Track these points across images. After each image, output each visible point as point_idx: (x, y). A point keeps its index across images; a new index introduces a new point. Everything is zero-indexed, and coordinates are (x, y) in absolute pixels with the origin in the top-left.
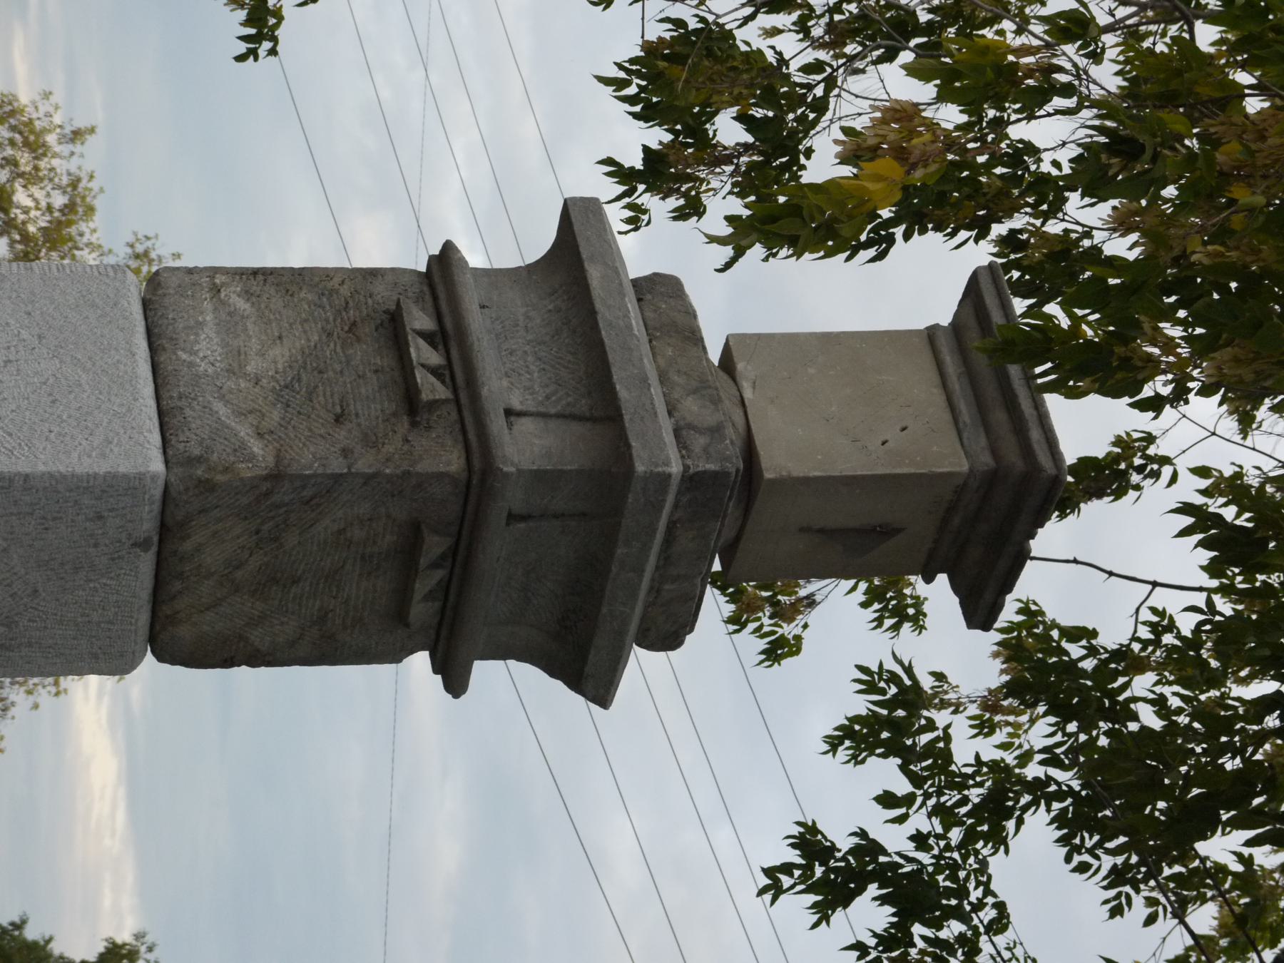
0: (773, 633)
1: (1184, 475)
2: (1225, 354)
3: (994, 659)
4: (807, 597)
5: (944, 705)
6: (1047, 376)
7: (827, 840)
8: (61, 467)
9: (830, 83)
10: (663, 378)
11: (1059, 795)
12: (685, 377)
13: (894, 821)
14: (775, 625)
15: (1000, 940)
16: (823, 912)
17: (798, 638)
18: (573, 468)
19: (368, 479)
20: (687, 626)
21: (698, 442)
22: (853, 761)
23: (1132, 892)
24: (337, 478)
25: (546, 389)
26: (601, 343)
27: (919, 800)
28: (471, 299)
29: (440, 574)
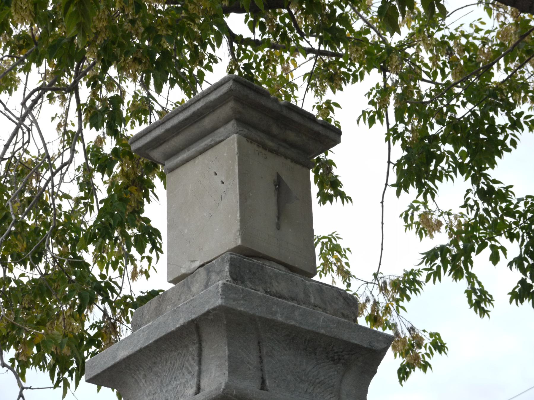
0: (430, 348)
3: (434, 237)
4: (410, 331)
6: (194, 114)
7: (517, 286)
12: (182, 295)
13: (505, 254)
14: (425, 347)
17: (431, 335)
18: (227, 349)
20: (340, 292)
22: (491, 302)
23: (524, 116)
25: (185, 374)
26: (156, 341)
27: (493, 243)
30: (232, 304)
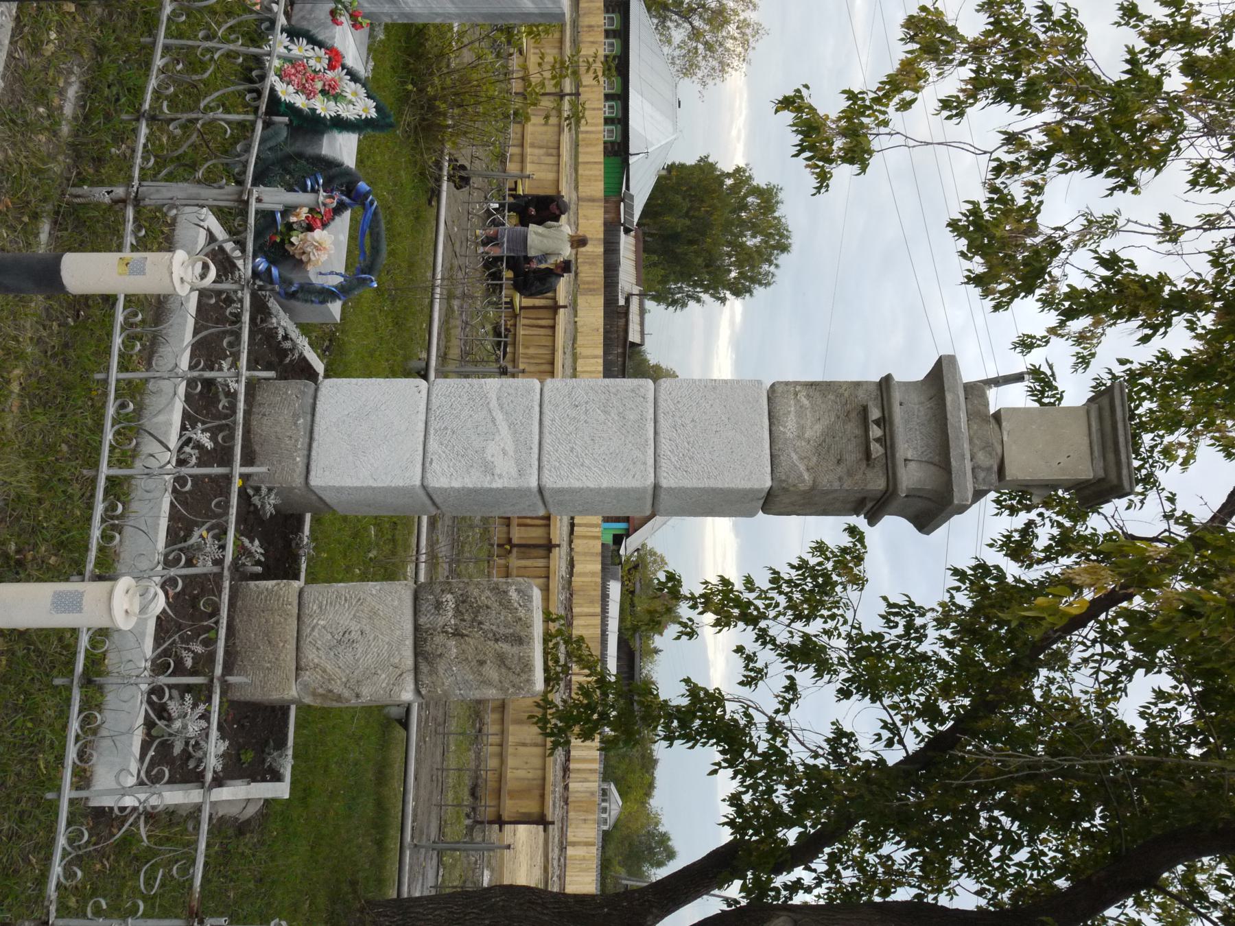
8: (732, 485)
21: (982, 475)
28: (897, 396)
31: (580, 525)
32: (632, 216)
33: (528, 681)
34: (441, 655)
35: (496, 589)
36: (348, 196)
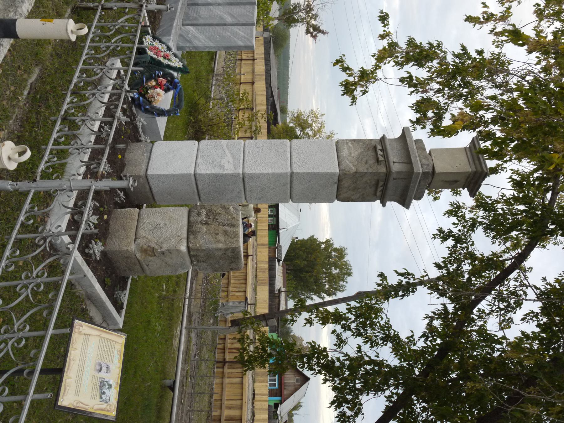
1: (508, 170)
2: (519, 153)
5: (464, 208)
9: (448, 106)
10: (419, 156)
11: (484, 224)
15: (473, 247)
16: (443, 242)
19: (371, 173)
21: (425, 167)
24: (366, 173)
28: (387, 144)
29: (382, 188)
30: (415, 174)
31: (258, 395)
32: (281, 254)
33: (237, 241)
34: (199, 232)
35: (224, 207)
36: (171, 85)
